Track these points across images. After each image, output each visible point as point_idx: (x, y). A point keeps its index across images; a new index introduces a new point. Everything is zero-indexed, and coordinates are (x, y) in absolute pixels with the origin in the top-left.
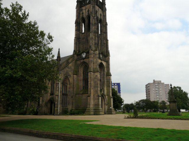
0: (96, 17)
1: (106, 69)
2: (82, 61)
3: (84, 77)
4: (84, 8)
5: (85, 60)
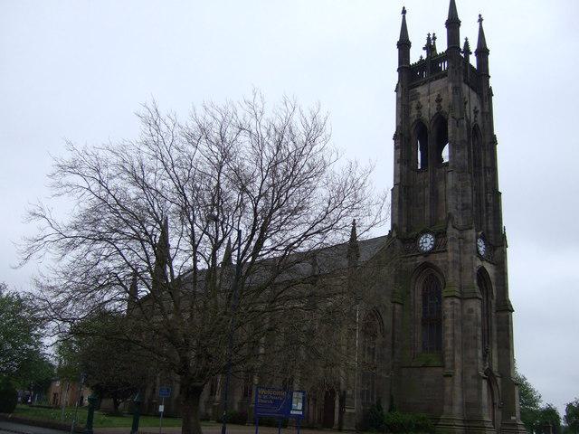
0: (465, 122)
1: (494, 287)
2: (420, 260)
3: (425, 313)
4: (421, 90)
5: (431, 259)
